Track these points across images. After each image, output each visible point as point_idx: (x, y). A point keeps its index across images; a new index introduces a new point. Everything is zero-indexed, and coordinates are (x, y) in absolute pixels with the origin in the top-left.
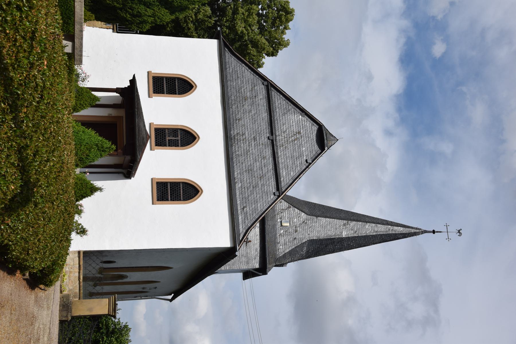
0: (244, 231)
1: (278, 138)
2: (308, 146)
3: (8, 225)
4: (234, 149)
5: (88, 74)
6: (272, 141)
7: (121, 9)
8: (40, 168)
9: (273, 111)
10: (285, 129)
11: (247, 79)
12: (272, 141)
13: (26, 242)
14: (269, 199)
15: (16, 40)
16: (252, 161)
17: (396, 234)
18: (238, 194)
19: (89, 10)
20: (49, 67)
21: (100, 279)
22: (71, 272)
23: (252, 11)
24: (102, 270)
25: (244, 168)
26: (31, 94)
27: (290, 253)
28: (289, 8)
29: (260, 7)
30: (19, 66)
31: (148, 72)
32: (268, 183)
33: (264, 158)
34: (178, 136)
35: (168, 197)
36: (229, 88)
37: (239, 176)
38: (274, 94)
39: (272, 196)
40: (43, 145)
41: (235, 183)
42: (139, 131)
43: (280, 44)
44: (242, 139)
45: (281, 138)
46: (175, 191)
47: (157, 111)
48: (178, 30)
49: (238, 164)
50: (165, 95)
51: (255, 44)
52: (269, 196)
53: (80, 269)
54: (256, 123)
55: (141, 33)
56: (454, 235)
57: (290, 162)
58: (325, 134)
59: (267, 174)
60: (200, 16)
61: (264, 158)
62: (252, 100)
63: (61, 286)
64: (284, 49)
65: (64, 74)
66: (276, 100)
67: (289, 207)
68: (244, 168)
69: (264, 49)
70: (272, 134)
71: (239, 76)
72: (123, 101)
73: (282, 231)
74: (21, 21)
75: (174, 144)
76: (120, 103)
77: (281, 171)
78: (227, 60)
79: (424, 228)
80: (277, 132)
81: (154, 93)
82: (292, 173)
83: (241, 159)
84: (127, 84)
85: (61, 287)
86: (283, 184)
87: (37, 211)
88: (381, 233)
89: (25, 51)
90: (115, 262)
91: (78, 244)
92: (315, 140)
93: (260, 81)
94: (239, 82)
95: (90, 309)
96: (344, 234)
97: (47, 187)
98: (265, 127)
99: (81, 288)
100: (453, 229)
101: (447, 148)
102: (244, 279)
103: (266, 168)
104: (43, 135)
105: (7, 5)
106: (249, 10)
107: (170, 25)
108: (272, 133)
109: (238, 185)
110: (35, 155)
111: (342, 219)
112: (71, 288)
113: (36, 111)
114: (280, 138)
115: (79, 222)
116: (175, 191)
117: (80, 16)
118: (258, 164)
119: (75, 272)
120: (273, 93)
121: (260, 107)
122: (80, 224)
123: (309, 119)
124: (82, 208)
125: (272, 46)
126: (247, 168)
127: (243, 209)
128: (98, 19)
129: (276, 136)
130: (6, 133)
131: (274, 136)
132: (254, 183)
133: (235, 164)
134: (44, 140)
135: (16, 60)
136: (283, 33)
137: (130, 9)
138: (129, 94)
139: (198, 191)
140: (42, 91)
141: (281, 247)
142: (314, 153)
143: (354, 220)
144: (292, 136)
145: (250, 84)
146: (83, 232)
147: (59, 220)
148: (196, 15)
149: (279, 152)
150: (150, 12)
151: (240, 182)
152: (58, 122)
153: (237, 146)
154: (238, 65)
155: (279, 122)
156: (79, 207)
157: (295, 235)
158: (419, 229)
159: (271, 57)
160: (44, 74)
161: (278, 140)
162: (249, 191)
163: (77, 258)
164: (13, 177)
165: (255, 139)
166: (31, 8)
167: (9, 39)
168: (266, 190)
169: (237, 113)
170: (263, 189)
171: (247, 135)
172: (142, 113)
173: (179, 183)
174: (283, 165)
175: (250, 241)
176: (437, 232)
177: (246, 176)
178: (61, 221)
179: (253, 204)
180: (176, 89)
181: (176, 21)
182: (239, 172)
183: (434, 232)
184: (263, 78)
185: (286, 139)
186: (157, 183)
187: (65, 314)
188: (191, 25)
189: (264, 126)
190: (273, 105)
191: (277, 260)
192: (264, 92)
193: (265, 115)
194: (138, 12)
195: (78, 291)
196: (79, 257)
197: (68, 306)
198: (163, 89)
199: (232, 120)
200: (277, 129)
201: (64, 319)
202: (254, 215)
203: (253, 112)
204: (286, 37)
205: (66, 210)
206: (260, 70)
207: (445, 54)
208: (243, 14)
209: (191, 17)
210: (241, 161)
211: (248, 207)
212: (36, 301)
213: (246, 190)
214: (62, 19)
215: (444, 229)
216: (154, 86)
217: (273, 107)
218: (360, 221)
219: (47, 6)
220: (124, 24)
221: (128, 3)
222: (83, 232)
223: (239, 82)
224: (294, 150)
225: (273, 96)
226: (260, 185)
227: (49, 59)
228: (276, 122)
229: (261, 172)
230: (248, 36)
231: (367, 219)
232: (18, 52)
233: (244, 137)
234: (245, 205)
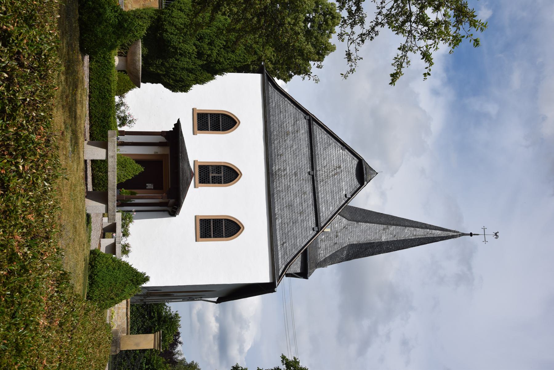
0: (284, 266)
1: (318, 173)
2: (348, 180)
4: (275, 185)
6: (313, 176)
7: (164, 75)
9: (314, 146)
10: (325, 165)
11: (289, 113)
12: (313, 176)
14: (308, 235)
16: (292, 197)
17: (434, 238)
25: (285, 203)
31: (193, 109)
32: (307, 218)
33: (305, 193)
34: (221, 173)
35: (211, 234)
36: (272, 123)
37: (280, 212)
38: (315, 127)
39: (311, 232)
41: (276, 219)
42: (183, 174)
43: (326, 48)
44: (283, 174)
45: (321, 172)
46: (218, 228)
47: (201, 148)
49: (279, 200)
50: (210, 131)
51: (301, 52)
52: (308, 232)
53: (127, 306)
54: (298, 158)
56: (491, 238)
57: (329, 197)
58: (364, 169)
59: (306, 209)
61: (305, 193)
62: (293, 135)
64: (331, 54)
66: (318, 134)
68: (285, 203)
71: (282, 110)
73: (323, 237)
75: (217, 181)
77: (321, 206)
78: (270, 95)
80: (318, 166)
82: (331, 208)
86: (322, 219)
88: (420, 237)
92: (355, 174)
93: (302, 115)
95: (137, 344)
96: (384, 239)
99: (129, 324)
100: (490, 231)
101: (492, 108)
103: (306, 203)
109: (278, 222)
111: (382, 224)
114: (321, 174)
116: (218, 228)
117: (112, 184)
118: (298, 199)
119: (123, 308)
120: (315, 127)
121: (302, 142)
123: (350, 153)
124: (129, 249)
126: (287, 204)
127: (283, 244)
129: (316, 171)
131: (315, 171)
132: (294, 219)
133: (276, 200)
136: (329, 37)
137: (173, 75)
138: (174, 138)
141: (322, 252)
142: (354, 187)
143: (394, 225)
144: (332, 171)
145: (293, 119)
149: (319, 187)
153: (278, 182)
155: (320, 156)
157: (336, 240)
162: (289, 226)
165: (296, 174)
168: (305, 226)
169: (279, 148)
170: (302, 225)
171: (288, 170)
172: (186, 153)
174: (323, 200)
176: (475, 235)
177: (286, 212)
179: (293, 239)
180: (219, 125)
182: (279, 207)
183: (471, 235)
185: (326, 174)
190: (314, 139)
192: (306, 126)
193: (306, 150)
194: (181, 78)
195: (125, 326)
197: (116, 342)
200: (317, 164)
203: (294, 147)
207: (492, 18)
210: (281, 196)
213: (286, 225)
215: (481, 232)
217: (314, 142)
218: (400, 225)
221: (171, 70)
224: (334, 184)
225: (315, 130)
226: (299, 221)
228: (317, 157)
229: (301, 208)
231: (406, 223)
233: (285, 172)
234: (284, 241)
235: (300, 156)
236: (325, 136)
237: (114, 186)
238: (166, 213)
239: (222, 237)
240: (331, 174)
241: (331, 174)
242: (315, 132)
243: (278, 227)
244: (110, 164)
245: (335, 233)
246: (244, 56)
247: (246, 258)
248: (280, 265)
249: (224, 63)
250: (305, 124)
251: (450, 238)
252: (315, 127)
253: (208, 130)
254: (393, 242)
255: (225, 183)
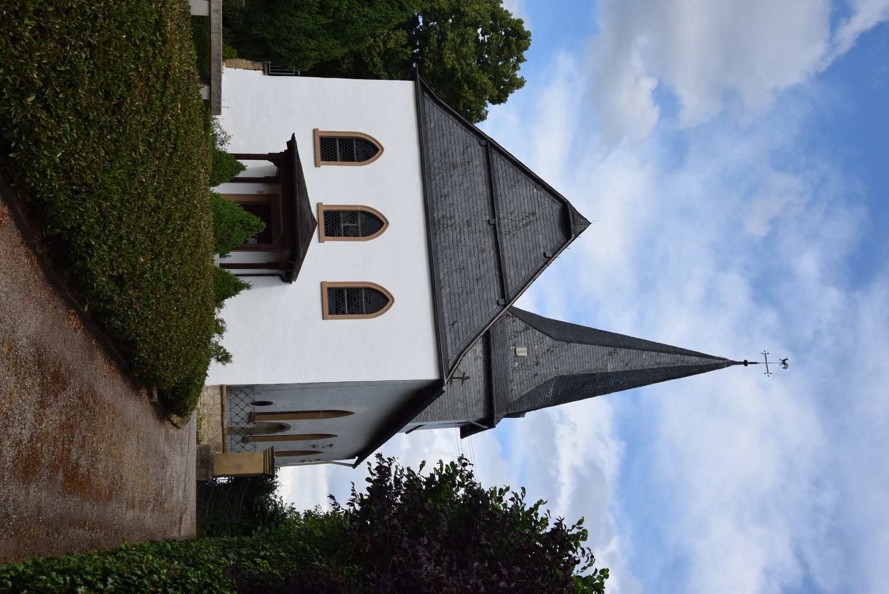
0: (455, 357)
1: (502, 221)
3: (136, 311)
4: (438, 239)
5: (228, 134)
6: (494, 225)
8: (172, 238)
10: (512, 210)
13: (157, 339)
14: (491, 310)
15: (148, 79)
18: (445, 303)
19: (230, 44)
20: (183, 110)
21: (250, 431)
22: (210, 415)
23: (466, 36)
24: (251, 417)
26: (163, 143)
27: (529, 396)
28: (523, 31)
29: (479, 30)
30: (151, 109)
31: (314, 131)
33: (483, 251)
37: (447, 277)
38: (496, 158)
39: (495, 306)
40: (176, 208)
41: (441, 288)
45: (506, 221)
46: (354, 301)
47: (328, 186)
48: (358, 68)
49: (445, 261)
51: (472, 84)
53: (223, 411)
55: (304, 74)
60: (391, 44)
61: (483, 251)
63: (197, 433)
64: (517, 92)
65: (200, 121)
67: (527, 329)
69: (485, 93)
70: (494, 217)
72: (279, 173)
74: (154, 58)
76: (274, 175)
77: (508, 270)
78: (427, 111)
79: (730, 358)
81: (322, 160)
82: (523, 273)
83: (449, 252)
84: (283, 148)
85: (197, 435)
87: (169, 296)
89: (158, 91)
90: (271, 403)
91: (217, 375)
93: (474, 140)
94: (445, 143)
95: (238, 467)
96: (610, 368)
97: (181, 264)
98: (483, 206)
102: (462, 437)
104: (176, 196)
105: (140, 40)
106: (462, 35)
107: (346, 61)
108: (493, 215)
109: (446, 291)
110: (167, 221)
112: (211, 436)
113: (169, 164)
114: (505, 224)
115: (220, 344)
116: (354, 301)
118: (473, 260)
120: (494, 156)
122: (222, 347)
125: (498, 88)
126: (457, 266)
127: (453, 325)
128: (241, 56)
129: (499, 219)
130: (136, 189)
134: (177, 202)
135: (149, 101)
136: (515, 67)
138: (287, 161)
139: (388, 300)
140: (175, 140)
141: (515, 387)
142: (556, 242)
143: (625, 347)
146: (225, 358)
147: (195, 315)
148: (385, 43)
149: (504, 242)
150: (313, 44)
151: (447, 286)
152: (193, 181)
153: (442, 235)
154: (443, 116)
156: (220, 323)
157: (536, 369)
158: (722, 359)
159: (497, 105)
160: (177, 119)
161: (502, 225)
162: (461, 298)
163: (219, 396)
164: (143, 246)
165: (469, 223)
166: (164, 42)
167: (141, 77)
171: (457, 218)
172: (305, 188)
173: (361, 289)
175: (468, 378)
176: (751, 363)
178: (198, 317)
181: (357, 55)
182: (445, 271)
183: (746, 363)
184: (480, 135)
186: (329, 289)
187: (204, 472)
188: (377, 60)
189: (482, 203)
190: (494, 173)
191: (509, 406)
193: (482, 188)
195: (220, 440)
196: (222, 395)
198: (336, 154)
199: (435, 197)
201: (203, 479)
202: (469, 333)
204: (519, 74)
205: (203, 302)
206: (480, 126)
208: (453, 40)
209: (379, 46)
211: (460, 322)
212: (167, 438)
214: (197, 54)
216: (322, 150)
217: (494, 178)
219: (181, 39)
220: (278, 62)
222: (225, 358)
223: (445, 143)
227: (183, 102)
230: (463, 73)
232: (151, 93)
233: (453, 221)
234: (455, 319)
235: (474, 198)
236: (511, 170)
237: (219, 55)
238: (277, 278)
239: (362, 313)
240: (521, 224)
241: (521, 224)
242: (495, 165)
243: (444, 300)
244: (213, 21)
245: (535, 360)
246: (387, 13)
247: (400, 348)
248: (450, 355)
249: (358, 22)
250: (481, 151)
251: (714, 369)
252: (495, 157)
253: (336, 160)
254: (624, 374)
255: (363, 235)
